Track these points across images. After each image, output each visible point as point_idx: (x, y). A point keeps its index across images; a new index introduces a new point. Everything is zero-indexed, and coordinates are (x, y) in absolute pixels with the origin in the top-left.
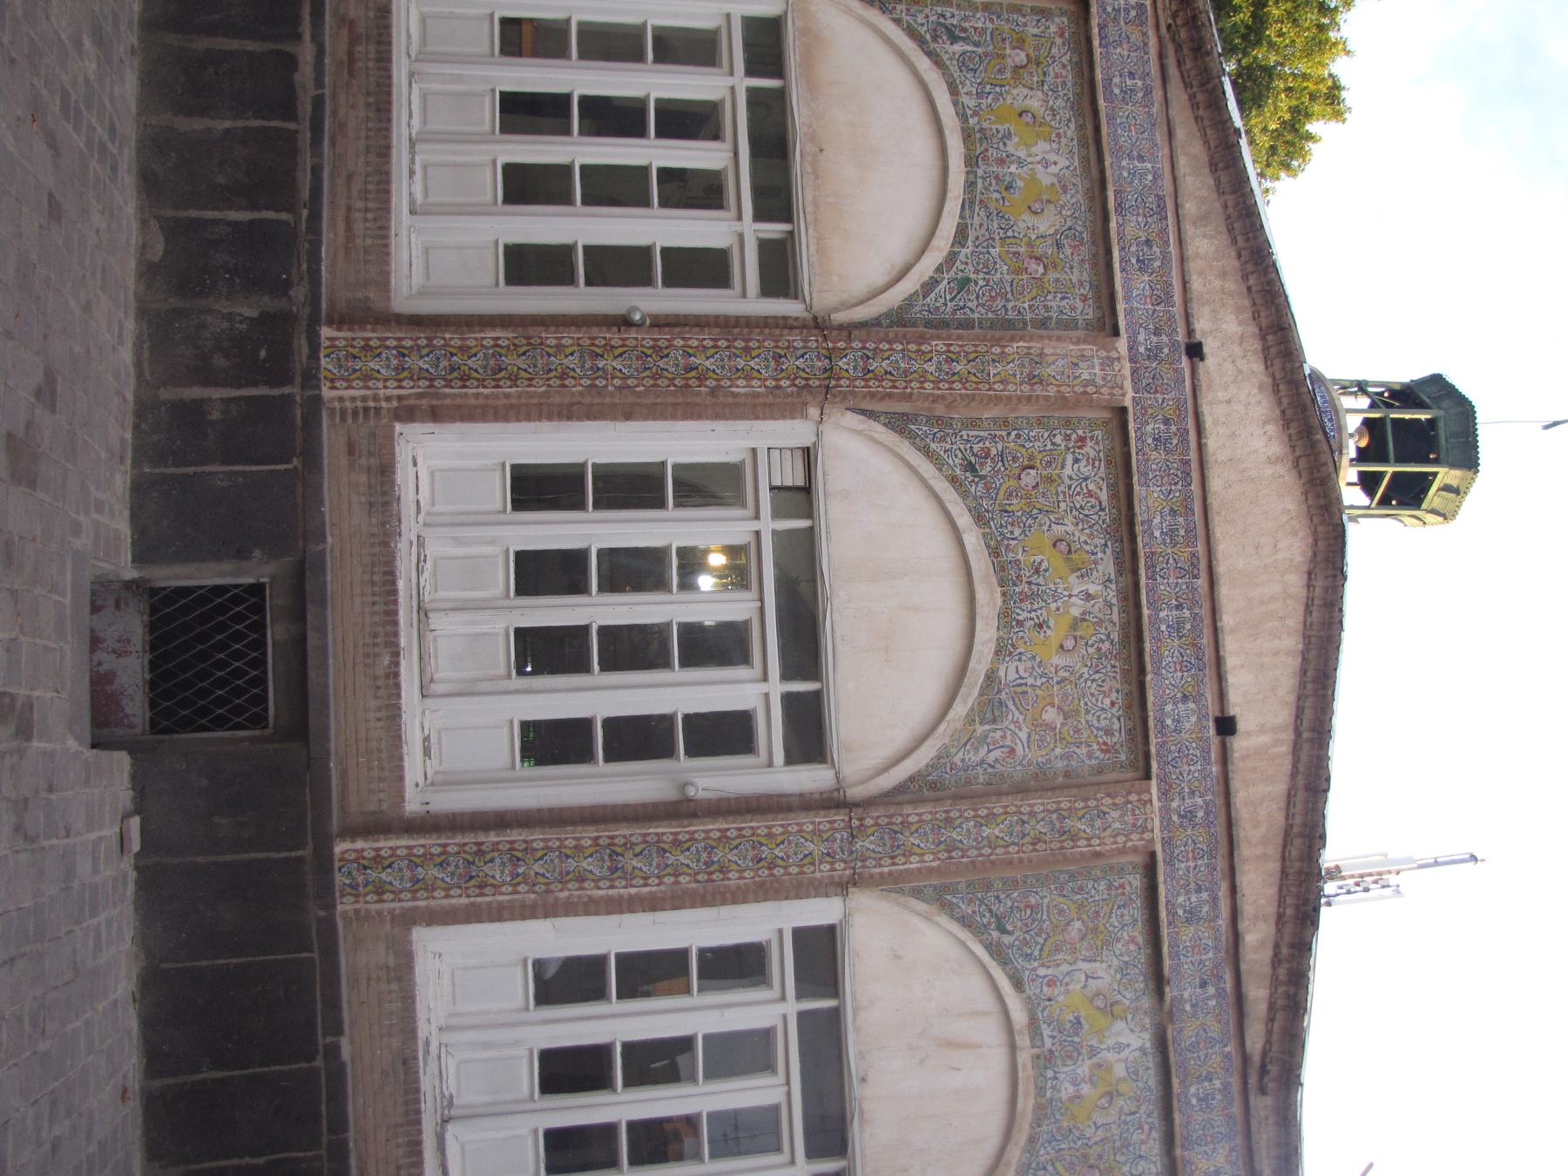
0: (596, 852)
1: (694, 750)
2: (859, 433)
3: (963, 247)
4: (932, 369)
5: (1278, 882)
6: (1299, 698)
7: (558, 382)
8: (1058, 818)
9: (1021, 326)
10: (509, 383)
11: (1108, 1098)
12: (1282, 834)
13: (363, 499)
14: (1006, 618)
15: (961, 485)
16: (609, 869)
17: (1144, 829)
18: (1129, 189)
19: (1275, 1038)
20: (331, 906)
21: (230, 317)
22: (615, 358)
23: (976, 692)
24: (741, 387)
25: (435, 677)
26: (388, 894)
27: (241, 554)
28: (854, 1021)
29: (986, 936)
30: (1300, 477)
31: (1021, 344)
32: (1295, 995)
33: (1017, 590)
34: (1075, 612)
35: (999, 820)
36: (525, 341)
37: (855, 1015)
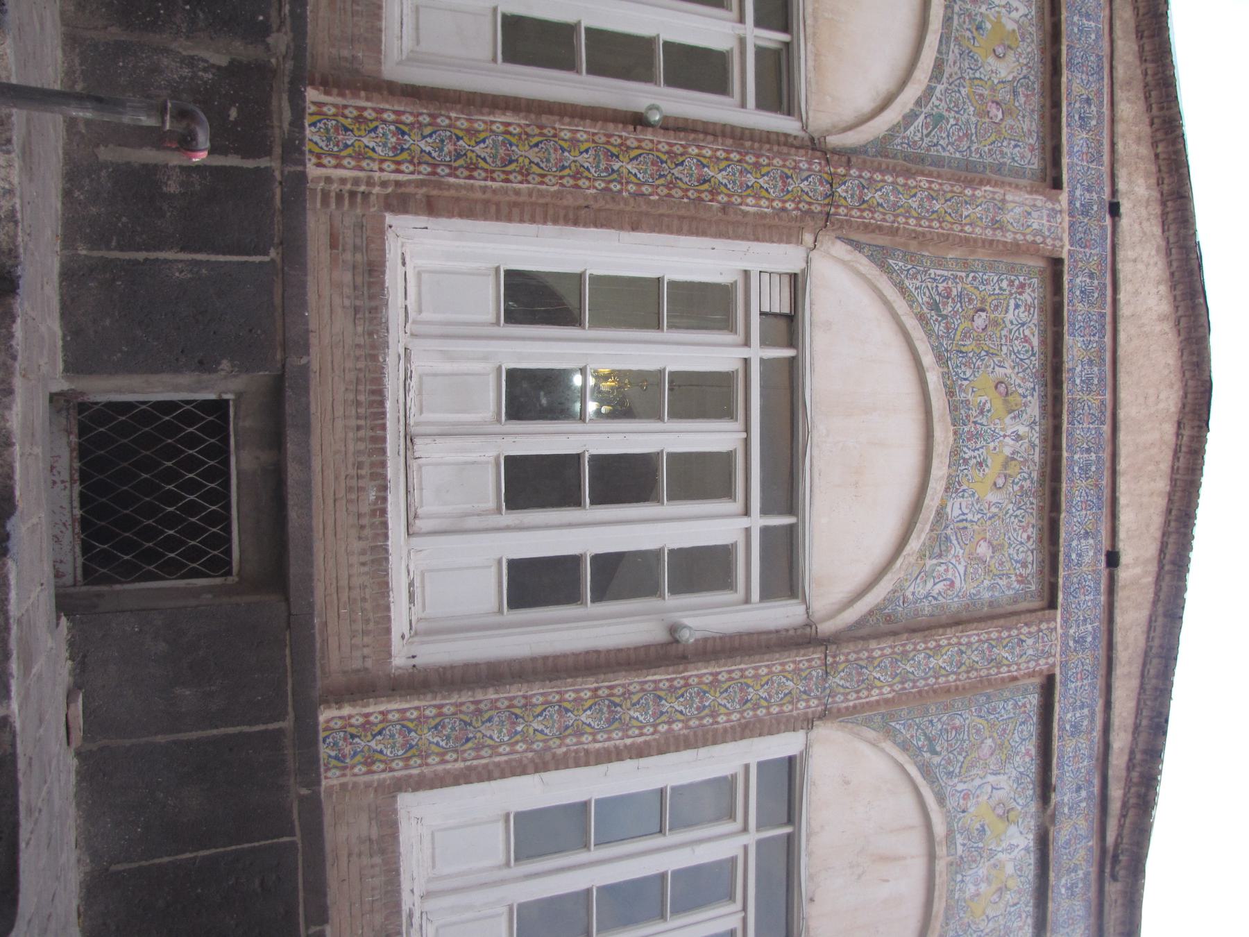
0: (595, 704)
2: (844, 263)
3: (939, 82)
6: (1164, 535)
7: (572, 182)
8: (988, 648)
9: (982, 169)
10: (519, 178)
11: (999, 893)
12: (1142, 655)
13: (347, 302)
17: (1050, 655)
19: (1126, 831)
21: (191, 62)
22: (631, 160)
23: (928, 527)
25: (419, 511)
26: (378, 764)
27: (205, 365)
28: (807, 845)
30: (1179, 335)
31: (988, 188)
32: (1146, 795)
34: (1007, 451)
35: (944, 651)
36: (537, 131)
37: (808, 840)
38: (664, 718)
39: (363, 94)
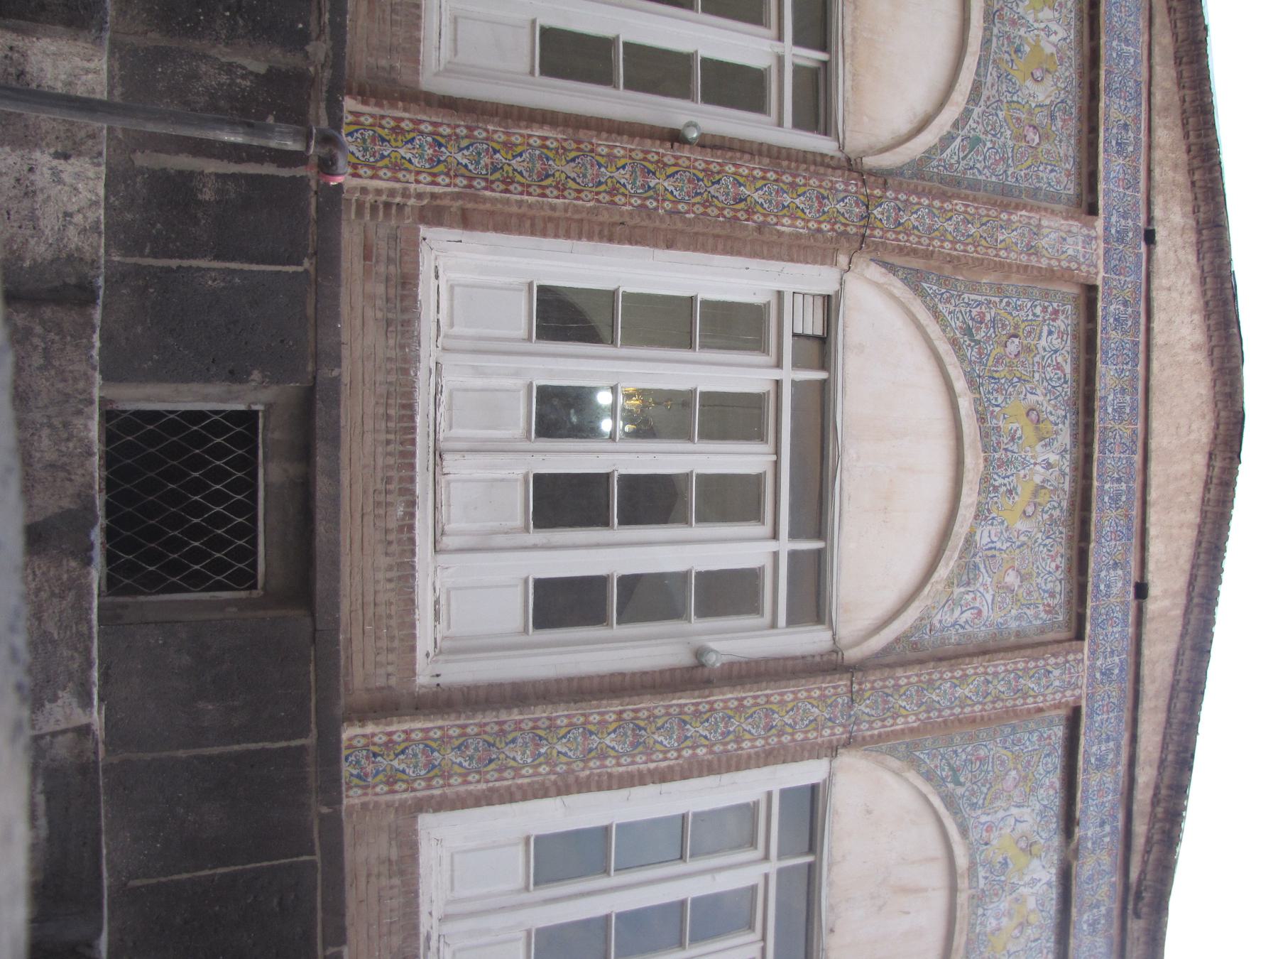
0: (620, 727)
1: (706, 610)
2: (877, 285)
3: (977, 105)
4: (950, 229)
5: (1162, 730)
6: (1193, 567)
7: (608, 198)
8: (1015, 678)
10: (556, 193)
13: (379, 315)
14: (986, 485)
15: (960, 349)
16: (632, 744)
18: (1116, 71)
19: (1150, 867)
21: (229, 68)
22: (668, 177)
23: (956, 556)
24: (786, 226)
25: (446, 528)
26: (400, 784)
27: (236, 376)
29: (943, 788)
30: (1212, 365)
31: (1024, 213)
33: (997, 456)
34: (1038, 480)
36: (574, 146)
37: (829, 870)
39: (400, 104)
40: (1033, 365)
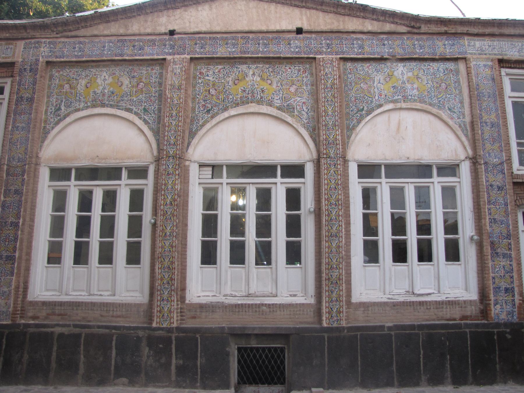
2: (195, 148)
3: (133, 110)
4: (174, 122)
5: (352, 17)
6: (291, 6)
7: (174, 248)
8: (327, 89)
9: (161, 91)
10: (174, 265)
11: (418, 79)
13: (211, 314)
14: (260, 102)
17: (332, 60)
19: (403, 22)
20: (344, 328)
21: (148, 357)
22: (166, 229)
23: (284, 114)
25: (270, 292)
27: (228, 354)
28: (389, 160)
31: (167, 92)
32: (389, 14)
33: (250, 98)
34: (259, 79)
35: (327, 109)
36: (160, 259)
37: (387, 160)
38: (337, 218)
39: (153, 311)
40: (219, 83)
